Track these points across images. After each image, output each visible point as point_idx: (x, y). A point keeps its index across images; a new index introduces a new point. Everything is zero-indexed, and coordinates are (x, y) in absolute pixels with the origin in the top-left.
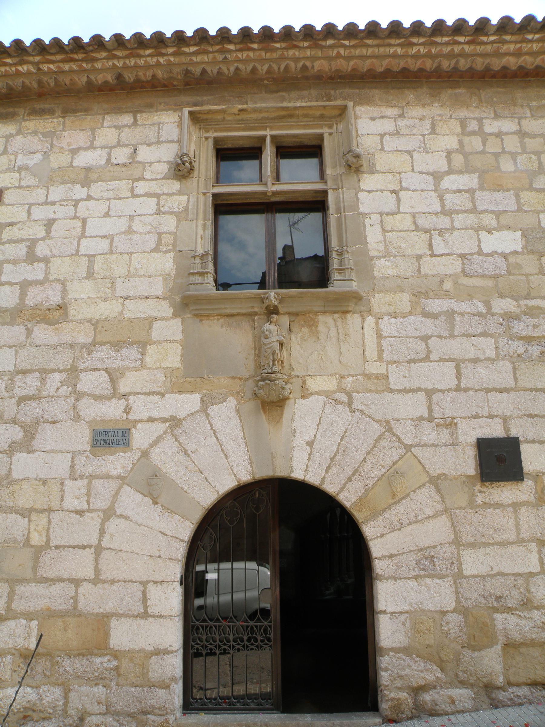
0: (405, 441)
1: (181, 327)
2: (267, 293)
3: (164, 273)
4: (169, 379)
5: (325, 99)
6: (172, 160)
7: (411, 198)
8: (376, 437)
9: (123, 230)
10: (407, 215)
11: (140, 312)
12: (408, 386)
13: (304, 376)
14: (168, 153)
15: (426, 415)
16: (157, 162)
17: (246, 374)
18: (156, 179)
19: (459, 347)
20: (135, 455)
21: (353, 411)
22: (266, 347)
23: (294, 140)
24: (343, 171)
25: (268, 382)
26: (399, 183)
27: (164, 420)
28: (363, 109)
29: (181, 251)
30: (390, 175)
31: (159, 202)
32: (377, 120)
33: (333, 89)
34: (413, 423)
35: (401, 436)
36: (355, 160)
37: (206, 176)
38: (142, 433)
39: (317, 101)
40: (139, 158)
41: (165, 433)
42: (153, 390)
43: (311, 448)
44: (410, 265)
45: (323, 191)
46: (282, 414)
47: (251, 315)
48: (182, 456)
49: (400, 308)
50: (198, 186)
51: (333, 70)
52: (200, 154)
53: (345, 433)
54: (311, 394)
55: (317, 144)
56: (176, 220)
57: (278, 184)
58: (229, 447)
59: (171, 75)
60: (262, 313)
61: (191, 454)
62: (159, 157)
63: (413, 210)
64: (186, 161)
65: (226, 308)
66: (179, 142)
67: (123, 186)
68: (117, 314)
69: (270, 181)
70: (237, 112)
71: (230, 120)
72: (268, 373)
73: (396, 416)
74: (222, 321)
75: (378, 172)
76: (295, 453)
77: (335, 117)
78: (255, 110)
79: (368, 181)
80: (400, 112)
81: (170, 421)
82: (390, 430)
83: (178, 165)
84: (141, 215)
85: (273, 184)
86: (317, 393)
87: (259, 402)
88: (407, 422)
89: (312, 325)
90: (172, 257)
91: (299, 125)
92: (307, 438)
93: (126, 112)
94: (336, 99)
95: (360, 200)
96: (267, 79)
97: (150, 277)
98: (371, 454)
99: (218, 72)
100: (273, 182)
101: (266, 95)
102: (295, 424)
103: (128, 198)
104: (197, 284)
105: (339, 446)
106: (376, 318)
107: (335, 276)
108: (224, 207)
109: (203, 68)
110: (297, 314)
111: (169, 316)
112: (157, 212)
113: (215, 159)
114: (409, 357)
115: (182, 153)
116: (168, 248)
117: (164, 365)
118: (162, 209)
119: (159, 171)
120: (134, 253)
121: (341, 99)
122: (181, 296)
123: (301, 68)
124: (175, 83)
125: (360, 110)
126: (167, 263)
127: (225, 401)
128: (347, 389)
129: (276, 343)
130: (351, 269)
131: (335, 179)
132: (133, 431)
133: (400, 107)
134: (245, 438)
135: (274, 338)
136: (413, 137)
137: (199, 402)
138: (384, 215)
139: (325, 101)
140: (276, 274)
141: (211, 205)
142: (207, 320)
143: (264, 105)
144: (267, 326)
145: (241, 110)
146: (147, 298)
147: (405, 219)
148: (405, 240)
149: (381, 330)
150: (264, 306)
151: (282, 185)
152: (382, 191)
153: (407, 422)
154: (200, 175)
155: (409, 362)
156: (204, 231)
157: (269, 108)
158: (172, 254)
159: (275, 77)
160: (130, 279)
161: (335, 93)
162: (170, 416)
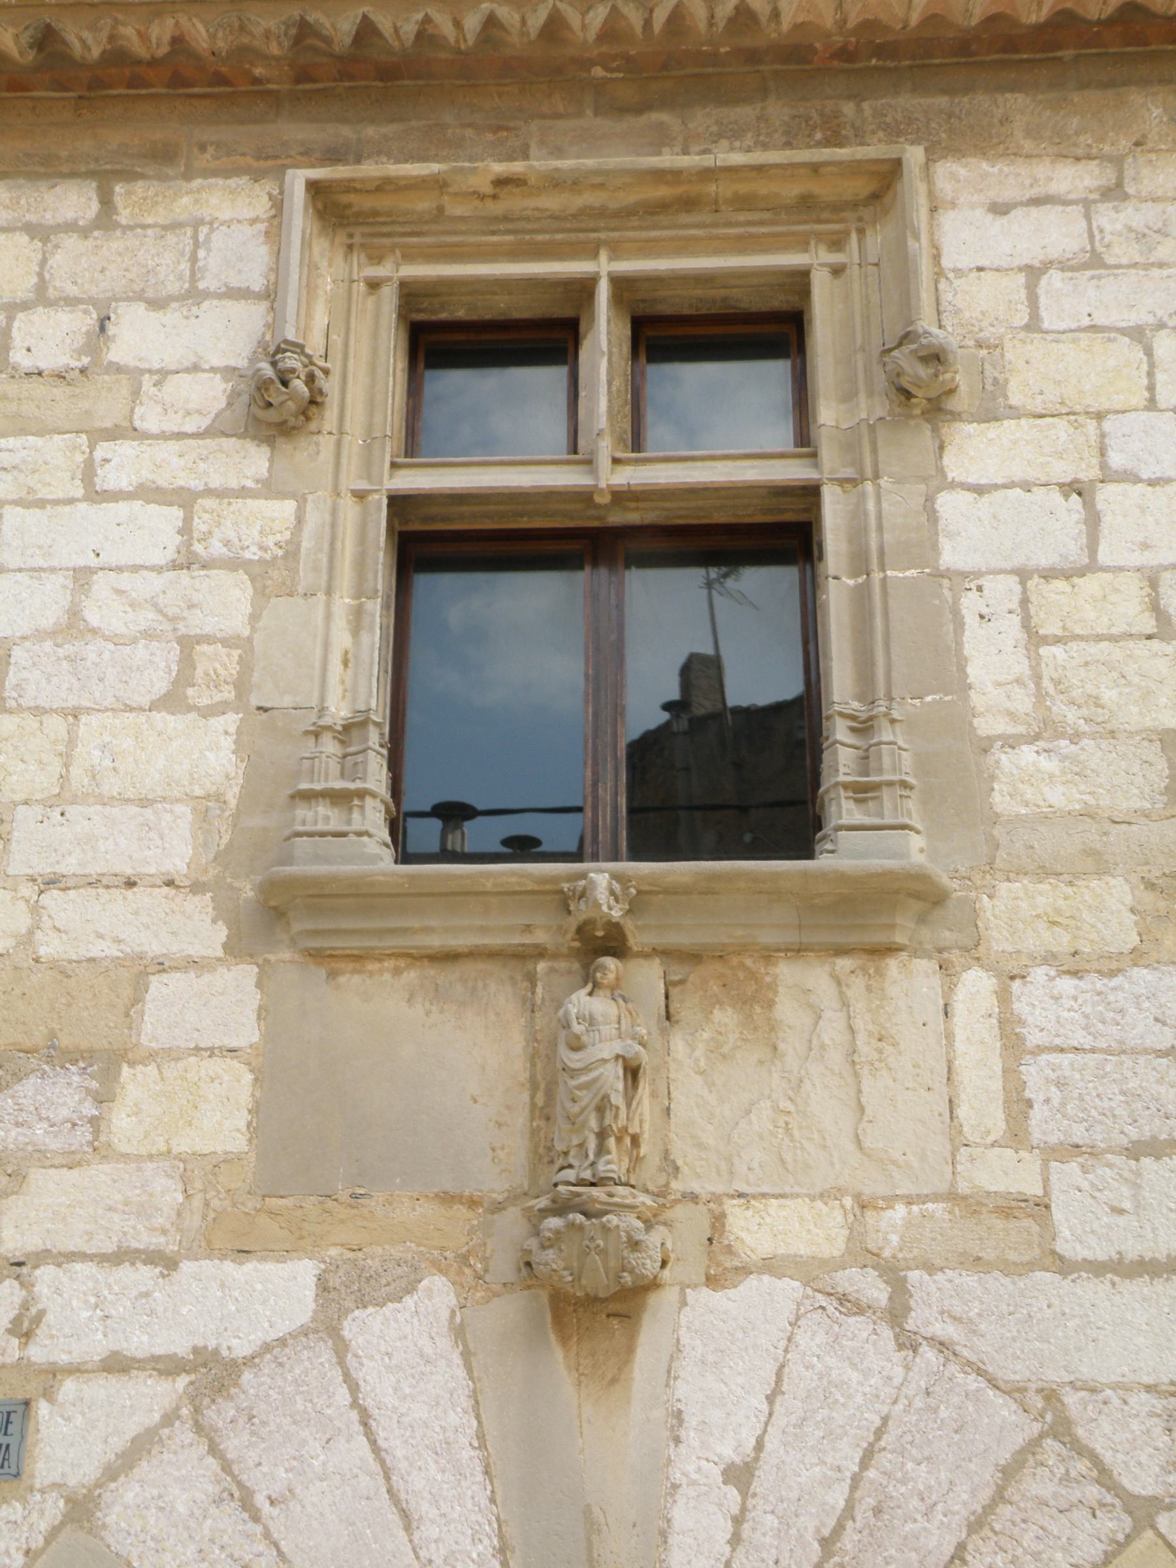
0: (1126, 1482)
1: (254, 999)
2: (583, 876)
3: (198, 792)
4: (197, 1202)
5: (818, 136)
6: (242, 363)
7: (1143, 510)
8: (1005, 1456)
9: (47, 622)
10: (1122, 577)
11: (101, 936)
12: (1133, 1250)
13: (717, 1198)
14: (227, 337)
16: (187, 370)
17: (495, 1185)
18: (180, 436)
20: (42, 1512)
21: (908, 1343)
22: (573, 1083)
23: (699, 292)
24: (880, 412)
25: (579, 1218)
26: (1095, 452)
27: (166, 1366)
28: (963, 172)
29: (266, 710)
30: (1061, 424)
31: (188, 520)
32: (1018, 212)
33: (849, 97)
34: (1158, 1404)
35: (1107, 1457)
36: (924, 372)
37: (369, 428)
38: (79, 1420)
39: (788, 145)
40: (117, 353)
41: (169, 1419)
42: (135, 1245)
43: (744, 1494)
44: (1136, 768)
45: (804, 488)
46: (630, 1350)
47: (522, 957)
48: (229, 1519)
49: (1094, 936)
50: (337, 464)
51: (850, 25)
52: (346, 344)
53: (879, 1433)
54: (745, 1271)
55: (785, 307)
56: (250, 591)
57: (637, 461)
58: (421, 1480)
59: (246, 40)
60: (565, 950)
61: (266, 1509)
62: (193, 349)
63: (1149, 559)
64: (293, 370)
65: (428, 930)
66: (271, 295)
67: (56, 456)
68: (10, 943)
69: (605, 448)
70: (488, 189)
71: (462, 219)
72: (581, 1183)
73: (1086, 1372)
74: (411, 976)
75: (1015, 413)
76: (680, 1515)
77: (855, 205)
78: (555, 182)
79: (974, 450)
80: (1108, 176)
81: (194, 1370)
82: (1062, 1429)
83: (263, 385)
84: (119, 569)
85: (616, 461)
86: (771, 1266)
87: (544, 1296)
88: (1133, 1400)
89: (754, 998)
90: (232, 729)
91: (718, 238)
92: (727, 1451)
93: (73, 175)
94: (860, 138)
95: (941, 525)
96: (603, 61)
97: (144, 802)
98: (986, 1531)
99: (420, 36)
100: (619, 455)
101: (599, 121)
102: (681, 1389)
103: (71, 501)
104: (322, 834)
105: (854, 1487)
106: (998, 975)
107: (842, 811)
108: (430, 546)
109: (365, 17)
110: (693, 957)
111: (209, 953)
112: (181, 560)
113: (402, 364)
114: (1133, 1133)
115: (279, 340)
116: (218, 697)
117: (182, 1145)
118: (198, 548)
119: (191, 406)
120: (88, 711)
121: (881, 134)
122: (259, 878)
123: (731, 20)
124: (258, 71)
125: (952, 174)
126: (210, 753)
127: (410, 1289)
128: (887, 1253)
129: (610, 1066)
130: (904, 785)
131: (850, 445)
132: (43, 1409)
133: (1110, 159)
134: (483, 1446)
135: (606, 1047)
136: (1156, 272)
137: (310, 1294)
138: (1036, 579)
139: (819, 144)
140: (623, 802)
141: (383, 539)
142: (355, 971)
143: (590, 162)
144: (580, 1001)
145: (501, 182)
146: (130, 884)
147: (1116, 591)
148: (1115, 674)
149: (1022, 1022)
150: (573, 923)
151: (648, 467)
152: (1027, 487)
153: (1133, 1400)
154: (347, 426)
155: (1135, 1151)
156: (356, 631)
157: (606, 173)
158: (231, 720)
159: (633, 53)
160: (71, 811)
161: (859, 110)
162: (196, 1350)
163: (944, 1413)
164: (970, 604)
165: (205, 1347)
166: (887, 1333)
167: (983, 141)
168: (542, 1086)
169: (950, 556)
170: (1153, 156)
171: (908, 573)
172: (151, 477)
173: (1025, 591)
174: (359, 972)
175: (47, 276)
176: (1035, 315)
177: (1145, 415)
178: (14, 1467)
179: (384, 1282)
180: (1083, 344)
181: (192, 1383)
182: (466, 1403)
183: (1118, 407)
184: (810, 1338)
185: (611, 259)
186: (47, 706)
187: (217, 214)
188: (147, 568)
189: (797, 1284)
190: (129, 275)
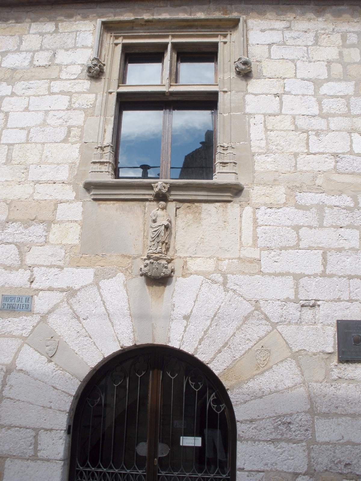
1: (81, 209)
12: (278, 271)
13: (186, 257)
15: (292, 297)
19: (327, 237)
21: (226, 290)
28: (255, 23)
31: (71, 99)
33: (229, 4)
41: (62, 301)
57: (176, 85)
79: (254, 85)
80: (288, 24)
82: (258, 308)
86: (197, 273)
102: (174, 299)
103: (45, 95)
105: (212, 321)
107: (218, 168)
114: (281, 244)
118: (73, 105)
119: (73, 73)
126: (72, 152)
127: (115, 276)
133: (288, 21)
136: (298, 47)
137: (92, 276)
152: (267, 94)
163: (233, 305)
164: (252, 121)
165: (70, 287)
166: (222, 288)
167: (262, 14)
168: (146, 231)
169: (248, 110)
170: (298, 21)
171: (238, 113)
172: (63, 89)
173: (265, 118)
174: (105, 204)
175: (43, 44)
176: (270, 55)
177: (294, 80)
178: (30, 308)
179: (109, 274)
180: (281, 62)
181: (66, 294)
182: (126, 300)
183: (288, 77)
184: (205, 289)
185: (172, 39)
186: (38, 142)
187: (82, 29)
188: (61, 110)
189: (202, 277)
190: (61, 43)
